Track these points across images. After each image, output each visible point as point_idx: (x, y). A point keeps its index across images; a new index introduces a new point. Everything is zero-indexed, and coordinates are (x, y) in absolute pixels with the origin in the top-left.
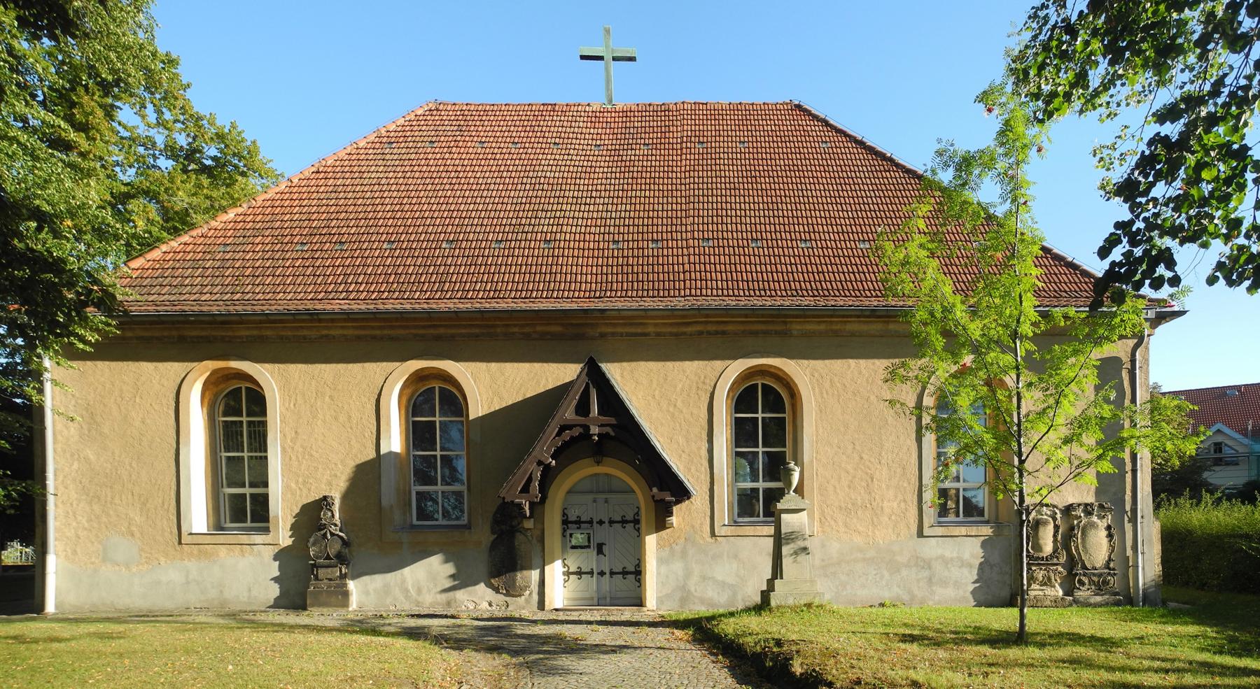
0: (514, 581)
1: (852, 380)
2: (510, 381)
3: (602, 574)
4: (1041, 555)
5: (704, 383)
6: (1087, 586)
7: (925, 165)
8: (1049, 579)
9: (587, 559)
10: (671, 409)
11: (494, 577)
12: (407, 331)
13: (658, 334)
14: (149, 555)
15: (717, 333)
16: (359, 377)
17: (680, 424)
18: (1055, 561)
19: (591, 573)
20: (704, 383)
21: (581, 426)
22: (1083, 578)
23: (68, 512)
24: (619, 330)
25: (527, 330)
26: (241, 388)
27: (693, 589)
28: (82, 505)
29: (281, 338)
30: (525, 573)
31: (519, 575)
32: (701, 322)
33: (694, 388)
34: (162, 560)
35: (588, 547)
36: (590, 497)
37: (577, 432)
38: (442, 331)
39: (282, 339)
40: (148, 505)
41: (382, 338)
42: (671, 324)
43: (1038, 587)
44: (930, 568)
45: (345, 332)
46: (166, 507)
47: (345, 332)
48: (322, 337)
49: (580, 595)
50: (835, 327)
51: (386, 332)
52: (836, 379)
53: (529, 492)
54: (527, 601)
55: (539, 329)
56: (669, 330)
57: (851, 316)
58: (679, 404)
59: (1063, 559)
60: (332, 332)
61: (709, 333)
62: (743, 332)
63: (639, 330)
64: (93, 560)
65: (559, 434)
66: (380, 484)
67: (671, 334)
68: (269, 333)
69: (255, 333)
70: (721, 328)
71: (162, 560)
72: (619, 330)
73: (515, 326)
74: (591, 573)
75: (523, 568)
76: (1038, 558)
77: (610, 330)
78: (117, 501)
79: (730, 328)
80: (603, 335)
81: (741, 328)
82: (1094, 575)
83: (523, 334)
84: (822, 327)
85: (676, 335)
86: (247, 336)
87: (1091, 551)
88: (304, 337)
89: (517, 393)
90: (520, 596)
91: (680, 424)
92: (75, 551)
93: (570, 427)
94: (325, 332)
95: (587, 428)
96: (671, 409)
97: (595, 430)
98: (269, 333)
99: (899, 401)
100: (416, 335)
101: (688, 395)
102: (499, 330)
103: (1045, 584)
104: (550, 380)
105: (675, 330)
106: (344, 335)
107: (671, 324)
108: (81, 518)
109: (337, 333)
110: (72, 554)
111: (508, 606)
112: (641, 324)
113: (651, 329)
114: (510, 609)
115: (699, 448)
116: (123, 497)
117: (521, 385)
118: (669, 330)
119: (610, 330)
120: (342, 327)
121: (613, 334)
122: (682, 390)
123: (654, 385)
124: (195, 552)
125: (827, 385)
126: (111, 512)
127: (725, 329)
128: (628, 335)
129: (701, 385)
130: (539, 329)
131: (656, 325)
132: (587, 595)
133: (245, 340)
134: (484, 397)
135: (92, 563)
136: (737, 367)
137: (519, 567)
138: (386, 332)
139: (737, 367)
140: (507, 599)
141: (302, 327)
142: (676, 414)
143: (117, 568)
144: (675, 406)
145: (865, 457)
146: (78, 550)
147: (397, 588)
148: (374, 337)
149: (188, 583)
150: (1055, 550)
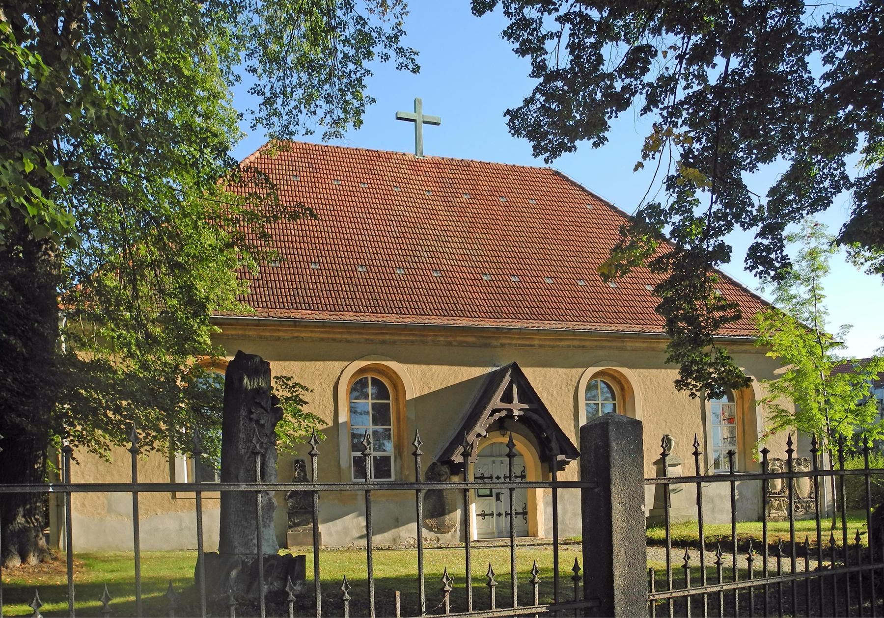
0: (444, 522)
1: (663, 379)
2: (436, 375)
3: (499, 515)
4: (775, 491)
5: (571, 380)
6: (800, 510)
7: (828, 13)
8: (781, 506)
9: (491, 504)
10: (550, 398)
11: (428, 518)
12: (361, 336)
13: (541, 346)
14: (147, 507)
15: (579, 347)
16: (321, 369)
17: (556, 408)
18: (783, 494)
19: (492, 515)
20: (571, 380)
21: (506, 410)
22: (798, 505)
23: (77, 472)
24: (514, 342)
25: (450, 339)
26: (388, 398)
27: (568, 522)
28: (89, 466)
29: (261, 337)
30: (451, 515)
31: (447, 517)
32: (570, 339)
33: (565, 384)
34: (159, 512)
35: (491, 495)
36: (491, 459)
37: (503, 414)
38: (387, 337)
39: (261, 338)
40: (146, 467)
41: (340, 341)
42: (550, 339)
43: (774, 511)
44: (713, 502)
45: (313, 335)
46: (161, 468)
47: (313, 335)
48: (294, 337)
49: (484, 531)
50: (652, 345)
51: (345, 336)
52: (654, 379)
53: (461, 454)
54: (453, 536)
55: (459, 338)
56: (548, 343)
57: (663, 339)
58: (555, 394)
59: (787, 494)
60: (302, 335)
61: (574, 346)
62: (596, 346)
63: (528, 343)
64: (99, 511)
65: (491, 415)
66: (339, 450)
67: (549, 346)
68: (251, 333)
69: (240, 332)
70: (583, 343)
71: (159, 512)
72: (514, 342)
73: (442, 336)
74: (492, 515)
75: (450, 512)
76: (774, 493)
77: (508, 341)
78: (120, 463)
79: (588, 344)
80: (503, 345)
81: (595, 343)
82: (804, 502)
83: (446, 342)
84: (645, 345)
85: (553, 347)
86: (232, 335)
87: (802, 487)
88: (279, 338)
89: (441, 384)
90: (448, 532)
91: (556, 408)
92: (83, 504)
93: (499, 410)
94: (296, 334)
95: (511, 411)
96: (550, 398)
97: (516, 413)
98: (251, 333)
99: (328, 552)
100: (366, 340)
101: (561, 388)
102: (430, 338)
103: (778, 510)
104: (465, 375)
105: (552, 343)
106: (311, 337)
107: (550, 339)
108: (88, 477)
109: (307, 335)
110: (81, 506)
111: (438, 540)
112: (530, 338)
113: (536, 342)
114: (440, 542)
115: (570, 425)
116: (125, 460)
117: (444, 378)
118: (548, 343)
119: (508, 341)
120: (312, 332)
121: (510, 344)
122: (557, 385)
123: (538, 381)
124: (187, 505)
125: (648, 383)
126: (115, 473)
127: (584, 344)
128: (520, 345)
129: (569, 382)
130: (459, 338)
131: (540, 339)
132: (489, 531)
133: (230, 337)
134: (417, 387)
135: (99, 514)
136: (592, 371)
137: (447, 511)
138: (345, 336)
139: (592, 371)
140: (438, 535)
141: (279, 330)
142: (553, 401)
143: (120, 518)
144: (552, 395)
145: (673, 430)
146: (86, 503)
147: (354, 531)
148: (334, 340)
149: (182, 529)
150: (783, 488)
